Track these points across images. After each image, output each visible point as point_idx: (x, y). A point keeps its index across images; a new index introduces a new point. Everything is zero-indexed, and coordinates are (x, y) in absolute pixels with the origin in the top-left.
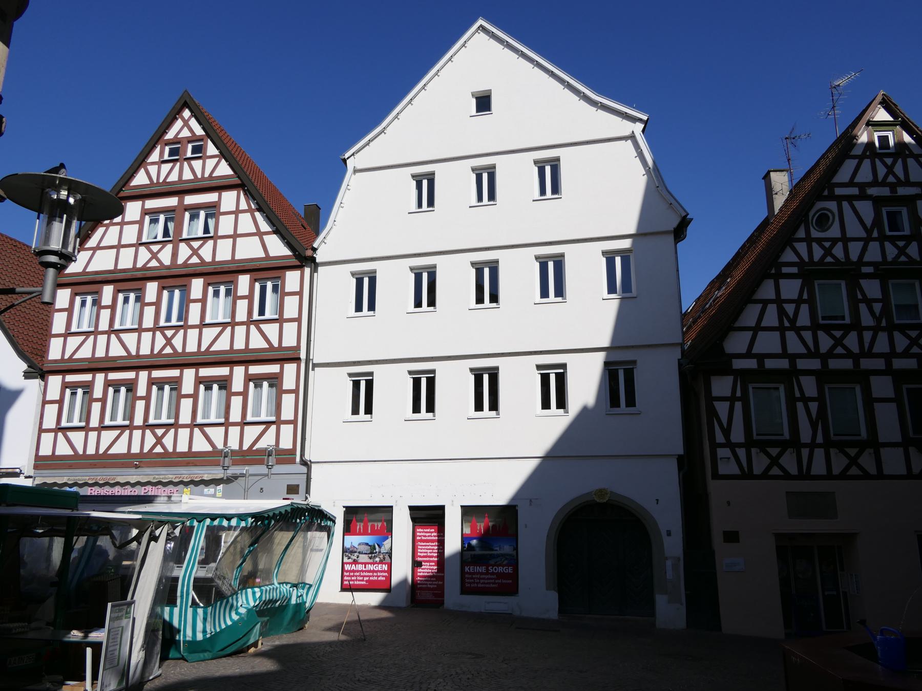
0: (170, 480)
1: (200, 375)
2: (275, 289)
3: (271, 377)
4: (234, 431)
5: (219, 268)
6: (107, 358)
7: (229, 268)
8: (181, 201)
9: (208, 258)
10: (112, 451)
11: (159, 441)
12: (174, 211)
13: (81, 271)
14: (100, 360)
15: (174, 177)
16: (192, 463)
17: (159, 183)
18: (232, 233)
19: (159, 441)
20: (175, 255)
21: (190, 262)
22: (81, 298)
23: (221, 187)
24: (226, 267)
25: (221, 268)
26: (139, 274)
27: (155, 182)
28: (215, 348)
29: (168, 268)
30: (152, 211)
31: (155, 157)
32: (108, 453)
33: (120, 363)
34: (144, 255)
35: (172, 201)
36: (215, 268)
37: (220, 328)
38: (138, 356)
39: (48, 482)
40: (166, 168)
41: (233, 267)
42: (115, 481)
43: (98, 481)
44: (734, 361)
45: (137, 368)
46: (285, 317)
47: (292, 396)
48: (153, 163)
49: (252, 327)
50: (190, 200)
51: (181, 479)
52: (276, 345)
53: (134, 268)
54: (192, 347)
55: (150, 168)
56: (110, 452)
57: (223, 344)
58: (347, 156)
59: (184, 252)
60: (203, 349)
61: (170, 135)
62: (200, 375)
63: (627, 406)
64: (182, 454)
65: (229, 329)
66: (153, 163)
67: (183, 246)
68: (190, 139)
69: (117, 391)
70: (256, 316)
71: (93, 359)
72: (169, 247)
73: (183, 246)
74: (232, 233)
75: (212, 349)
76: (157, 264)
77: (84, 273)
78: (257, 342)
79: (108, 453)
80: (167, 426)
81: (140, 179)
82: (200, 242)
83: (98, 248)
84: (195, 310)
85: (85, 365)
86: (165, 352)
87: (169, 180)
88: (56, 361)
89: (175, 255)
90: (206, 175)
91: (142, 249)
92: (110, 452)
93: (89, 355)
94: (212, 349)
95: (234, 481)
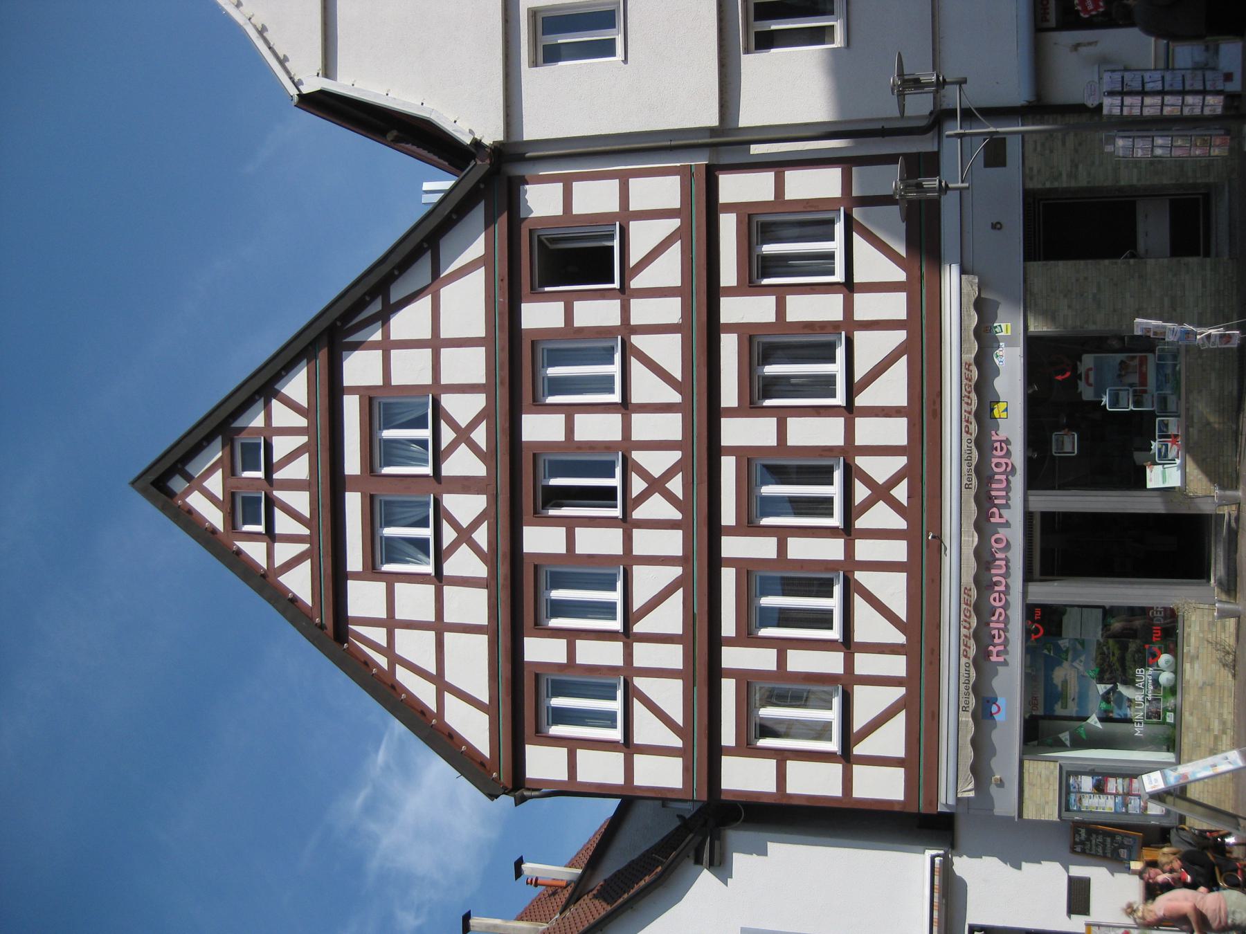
0: (970, 690)
1: (735, 404)
2: (561, 581)
3: (746, 231)
4: (865, 664)
5: (503, 373)
6: (686, 639)
7: (502, 349)
8: (356, 483)
9: (478, 402)
10: (900, 609)
11: (881, 492)
12: (372, 497)
13: (486, 717)
14: (689, 657)
15: (300, 501)
16: (934, 403)
17: (311, 536)
18: (431, 635)
19: (881, 492)
20: (465, 485)
21: (483, 446)
22: (545, 478)
23: (335, 390)
24: (503, 356)
25: (501, 369)
26: (503, 570)
27: (307, 546)
28: (677, 713)
29: (493, 501)
30: (369, 530)
31: (256, 551)
32: (904, 619)
33: (701, 607)
34: (464, 563)
35: (353, 502)
36: (502, 383)
37: (633, 360)
38: (683, 561)
39: (974, 517)
40: (284, 524)
41: (502, 339)
42: (973, 586)
43: (973, 383)
44: (752, 147)
45: (715, 562)
46: (620, 552)
47: (793, 423)
48: (270, 555)
49: (638, 628)
50: (352, 464)
51: (972, 419)
52: (677, 571)
53: (489, 583)
54: (670, 427)
55: (279, 561)
56: (902, 614)
57: (670, 695)
58: (293, 92)
59: (463, 463)
60: (677, 742)
61: (215, 518)
62: (735, 404)
63: (835, 397)
64: (915, 431)
65: (636, 340)
66: (270, 555)
67: (450, 468)
68: (229, 470)
69: (767, 730)
70: (617, 512)
71: (686, 674)
72: (449, 501)
73: (450, 468)
74: (431, 635)
75: (679, 720)
76: (482, 427)
77: (490, 709)
78: (670, 617)
79: (904, 619)
80: (850, 473)
81: (299, 583)
82: (444, 426)
83: (438, 680)
84: (592, 653)
85: (701, 691)
86: (679, 493)
87: (306, 512)
88: (687, 770)
89: (465, 485)
90: (302, 422)
91: (449, 569)
92: (903, 615)
93: (677, 685)
94: (679, 720)
95: (976, 109)
